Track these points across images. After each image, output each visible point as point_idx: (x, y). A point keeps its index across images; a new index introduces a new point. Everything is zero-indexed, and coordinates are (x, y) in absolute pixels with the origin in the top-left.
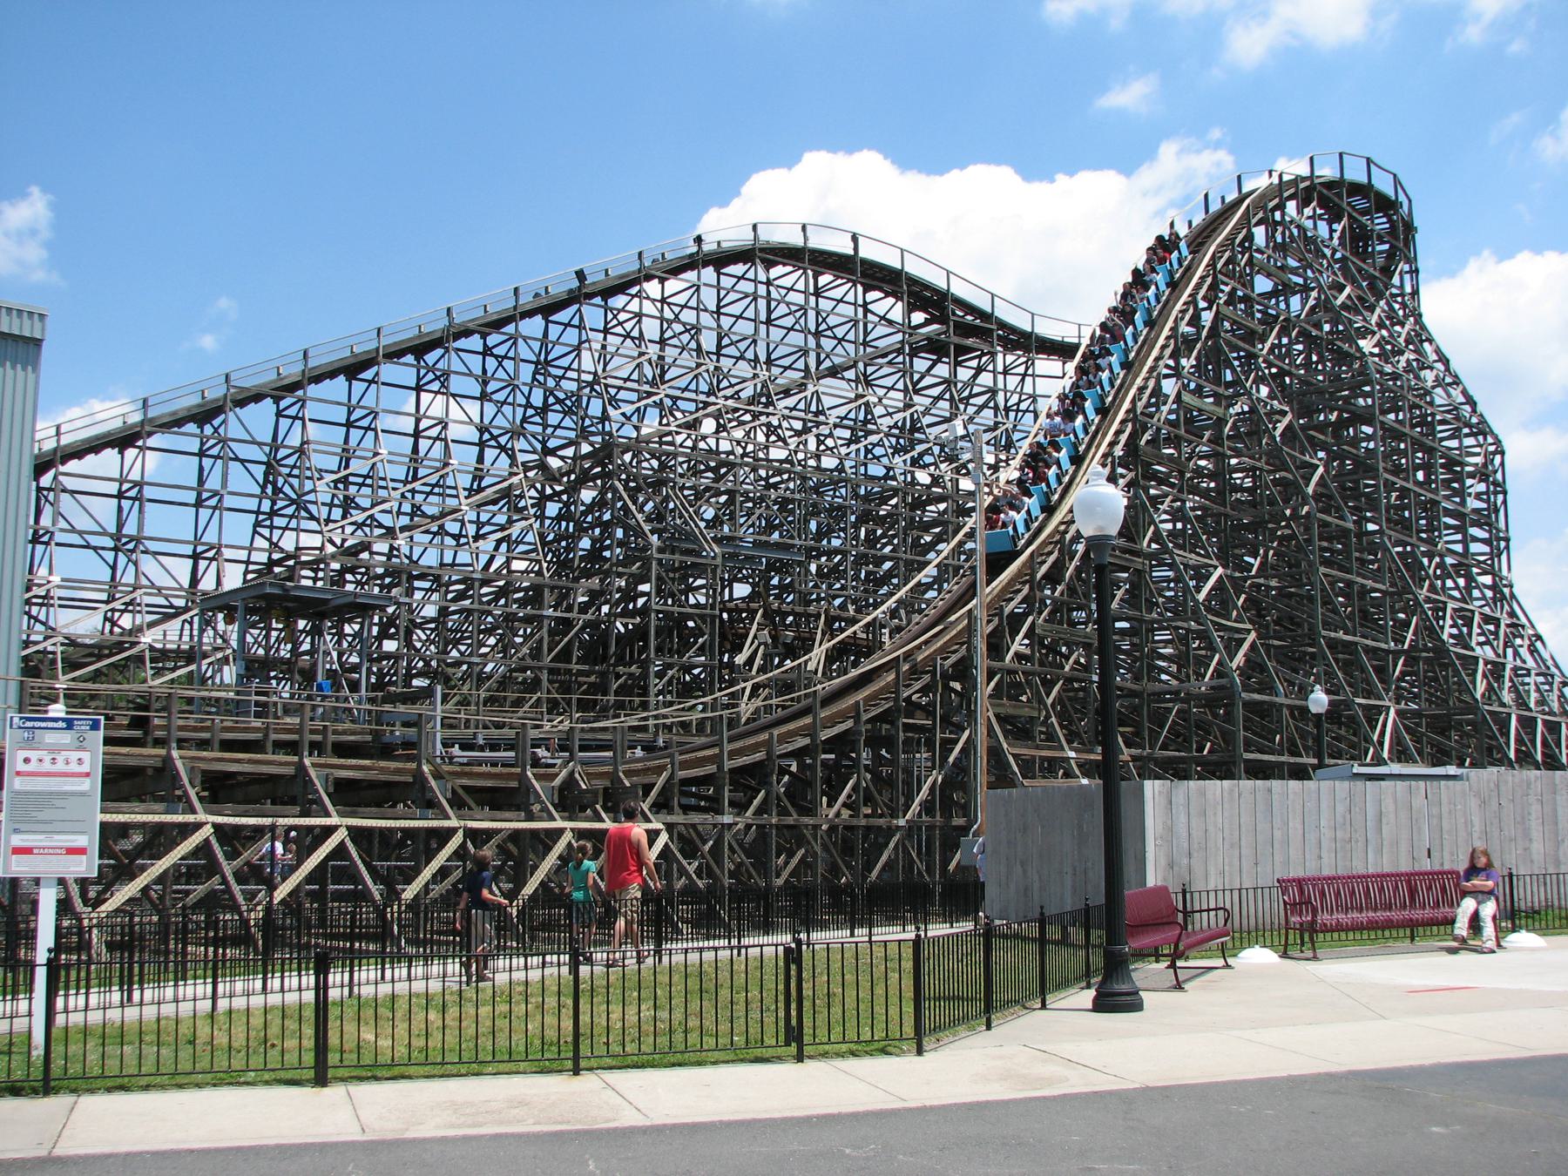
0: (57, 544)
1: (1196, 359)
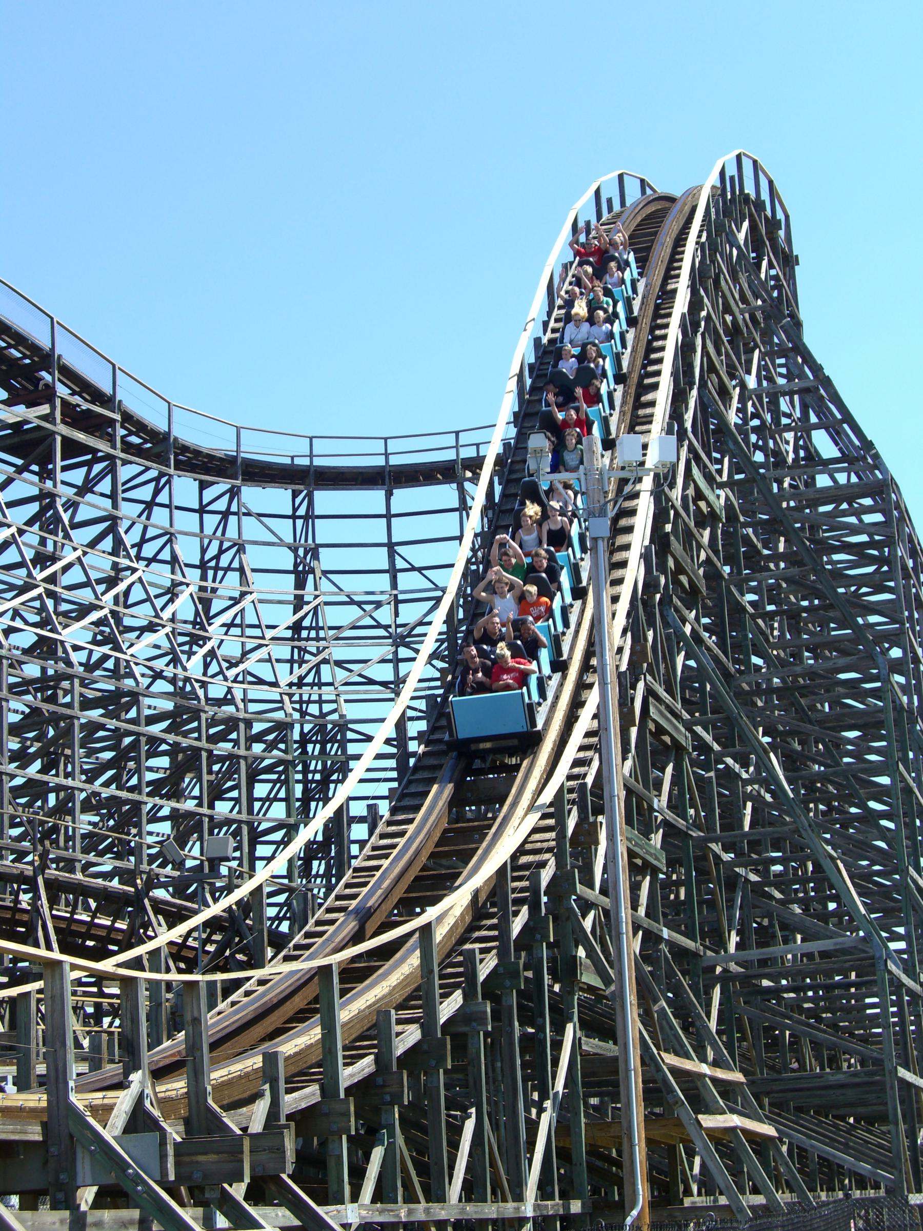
0: (171, 525)
1: (828, 845)
